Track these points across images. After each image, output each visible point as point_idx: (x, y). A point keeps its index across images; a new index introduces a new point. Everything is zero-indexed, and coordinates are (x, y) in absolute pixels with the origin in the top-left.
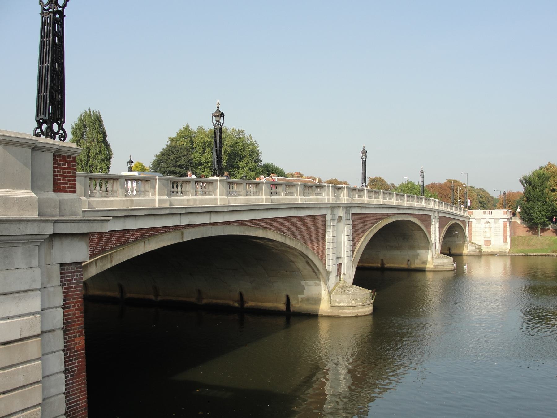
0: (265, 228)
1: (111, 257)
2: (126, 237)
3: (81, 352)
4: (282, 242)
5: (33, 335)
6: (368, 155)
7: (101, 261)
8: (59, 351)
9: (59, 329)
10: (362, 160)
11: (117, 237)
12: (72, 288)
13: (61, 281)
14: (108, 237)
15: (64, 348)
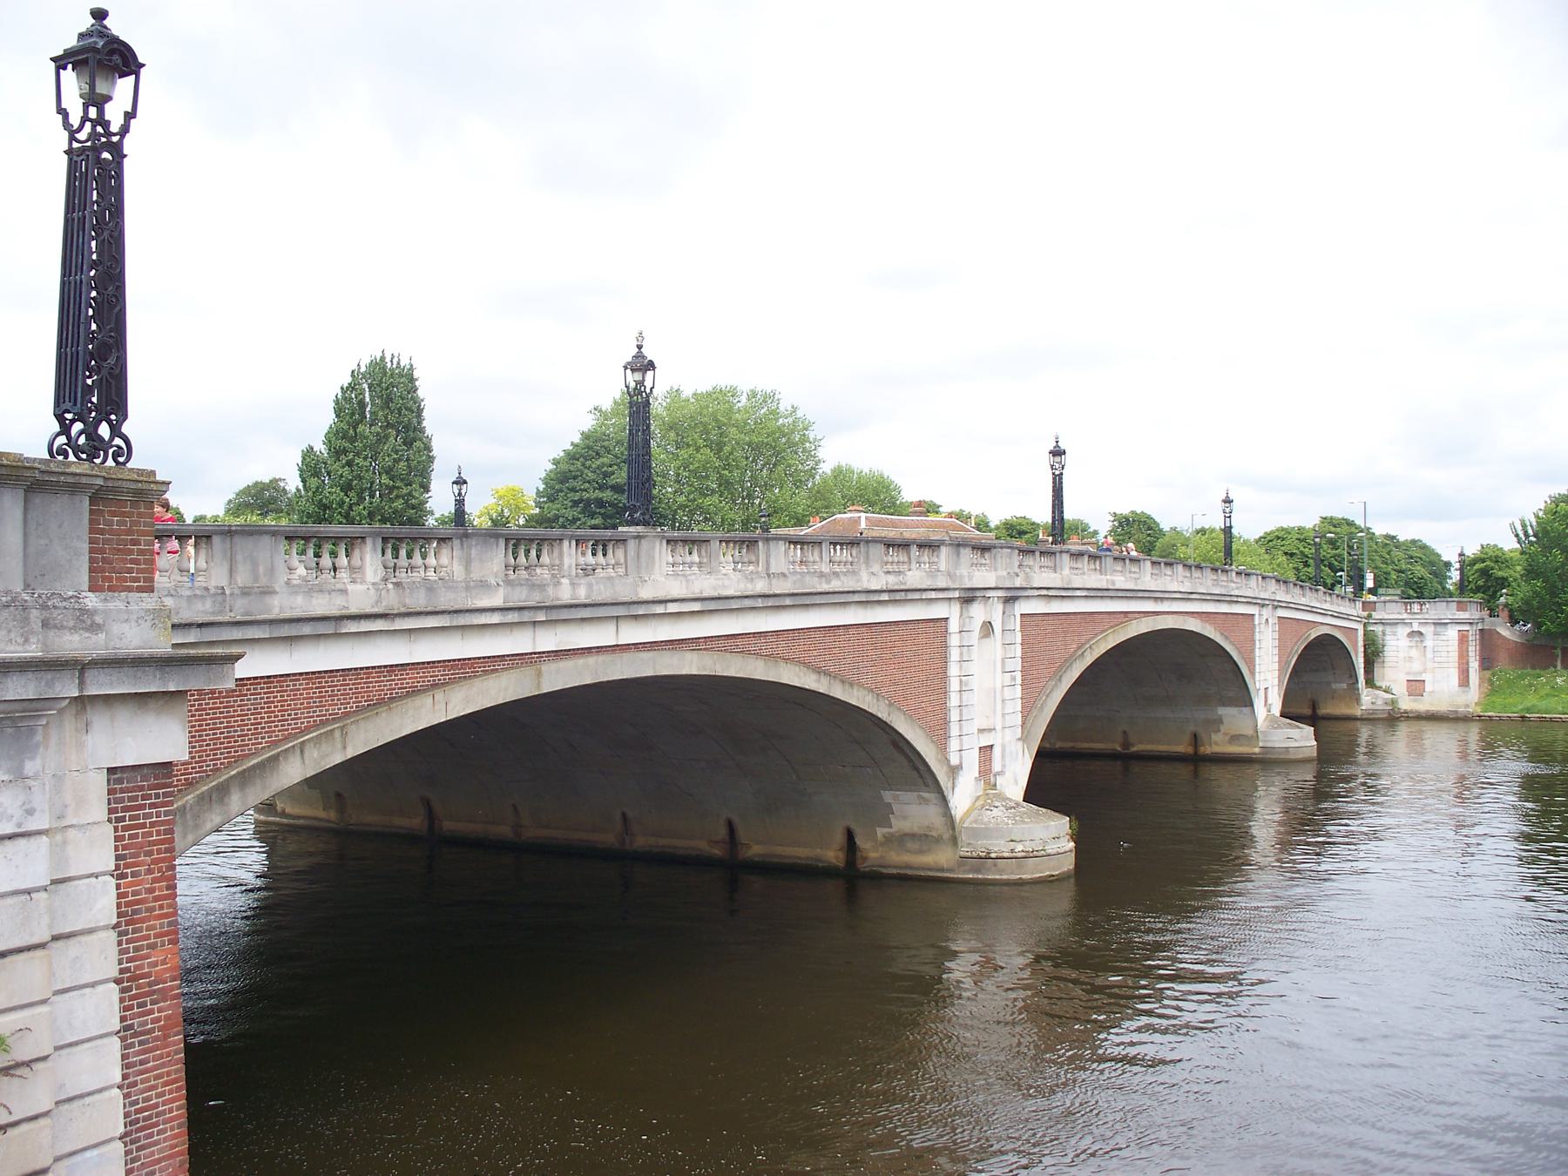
0: (772, 657)
1: (344, 735)
2: (385, 686)
3: (169, 984)
4: (821, 691)
5: (29, 944)
6: (1068, 459)
7: (315, 746)
10: (1053, 474)
11: (360, 683)
12: (143, 826)
14: (336, 686)
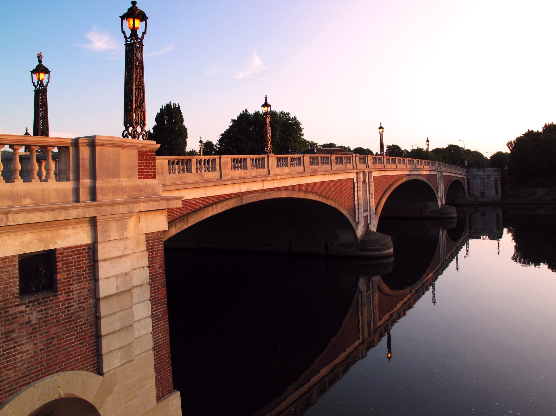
8: (147, 300)
9: (146, 283)
10: (380, 135)
12: (155, 251)
13: (147, 247)
15: (150, 298)
